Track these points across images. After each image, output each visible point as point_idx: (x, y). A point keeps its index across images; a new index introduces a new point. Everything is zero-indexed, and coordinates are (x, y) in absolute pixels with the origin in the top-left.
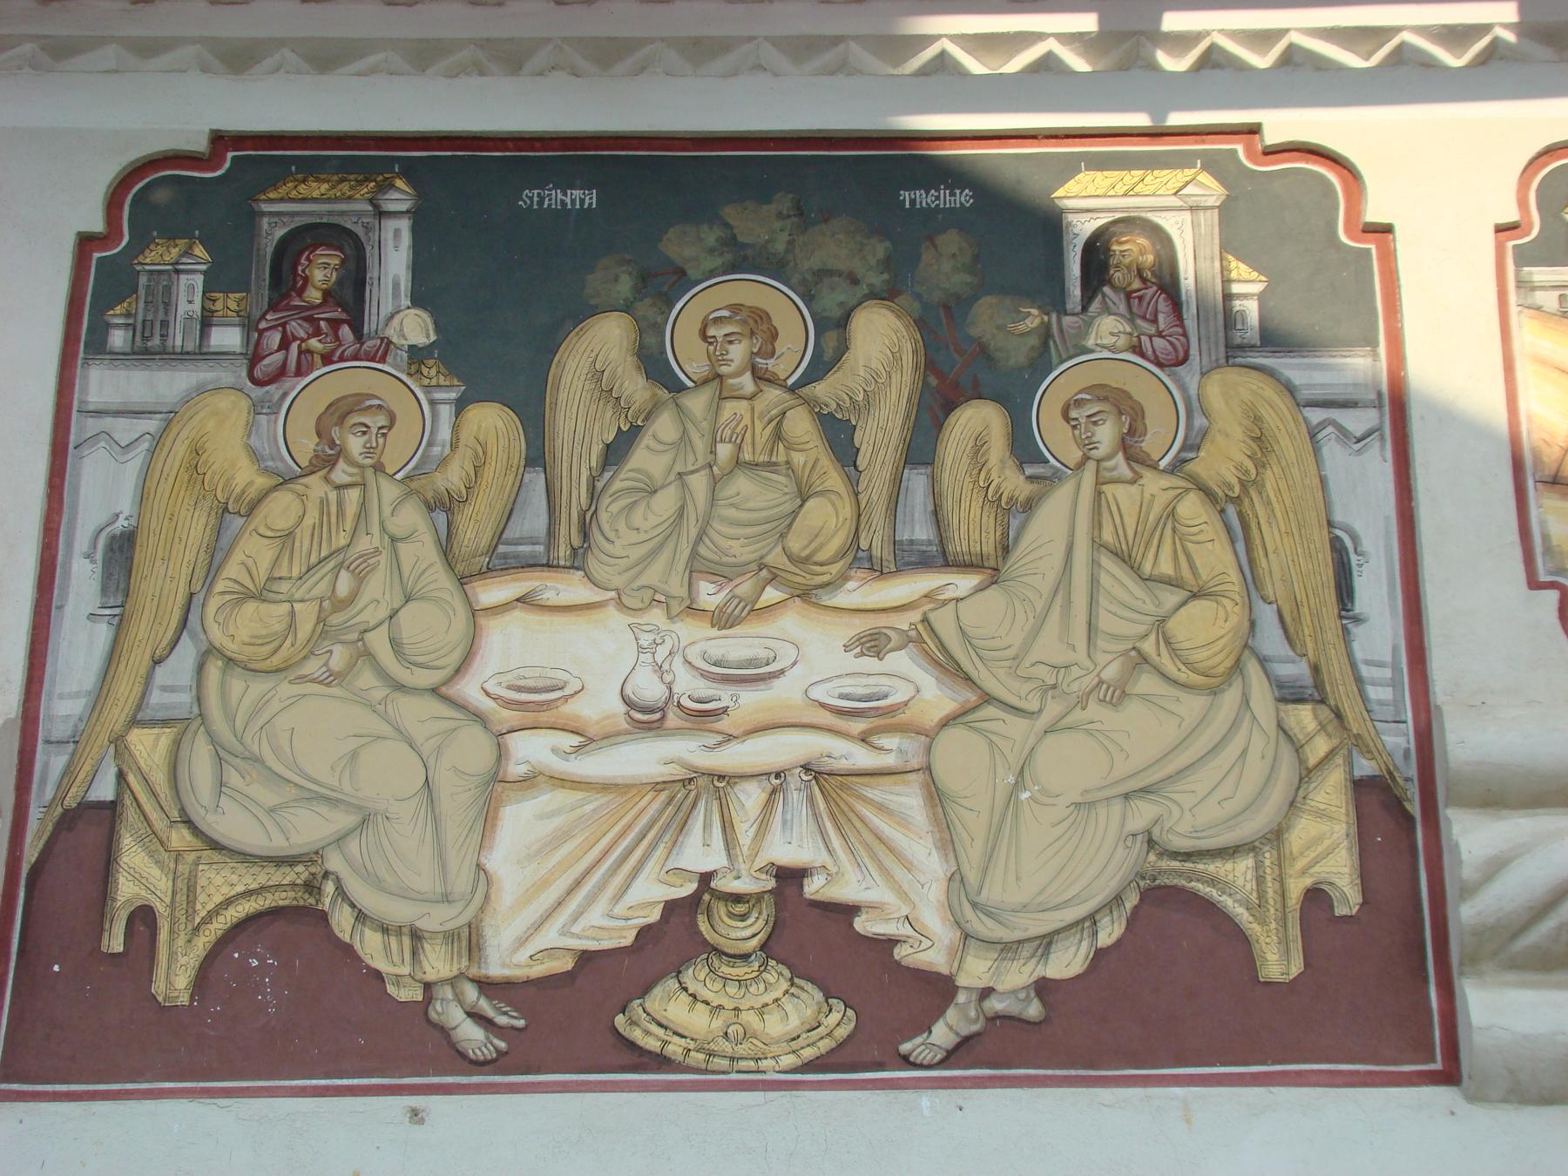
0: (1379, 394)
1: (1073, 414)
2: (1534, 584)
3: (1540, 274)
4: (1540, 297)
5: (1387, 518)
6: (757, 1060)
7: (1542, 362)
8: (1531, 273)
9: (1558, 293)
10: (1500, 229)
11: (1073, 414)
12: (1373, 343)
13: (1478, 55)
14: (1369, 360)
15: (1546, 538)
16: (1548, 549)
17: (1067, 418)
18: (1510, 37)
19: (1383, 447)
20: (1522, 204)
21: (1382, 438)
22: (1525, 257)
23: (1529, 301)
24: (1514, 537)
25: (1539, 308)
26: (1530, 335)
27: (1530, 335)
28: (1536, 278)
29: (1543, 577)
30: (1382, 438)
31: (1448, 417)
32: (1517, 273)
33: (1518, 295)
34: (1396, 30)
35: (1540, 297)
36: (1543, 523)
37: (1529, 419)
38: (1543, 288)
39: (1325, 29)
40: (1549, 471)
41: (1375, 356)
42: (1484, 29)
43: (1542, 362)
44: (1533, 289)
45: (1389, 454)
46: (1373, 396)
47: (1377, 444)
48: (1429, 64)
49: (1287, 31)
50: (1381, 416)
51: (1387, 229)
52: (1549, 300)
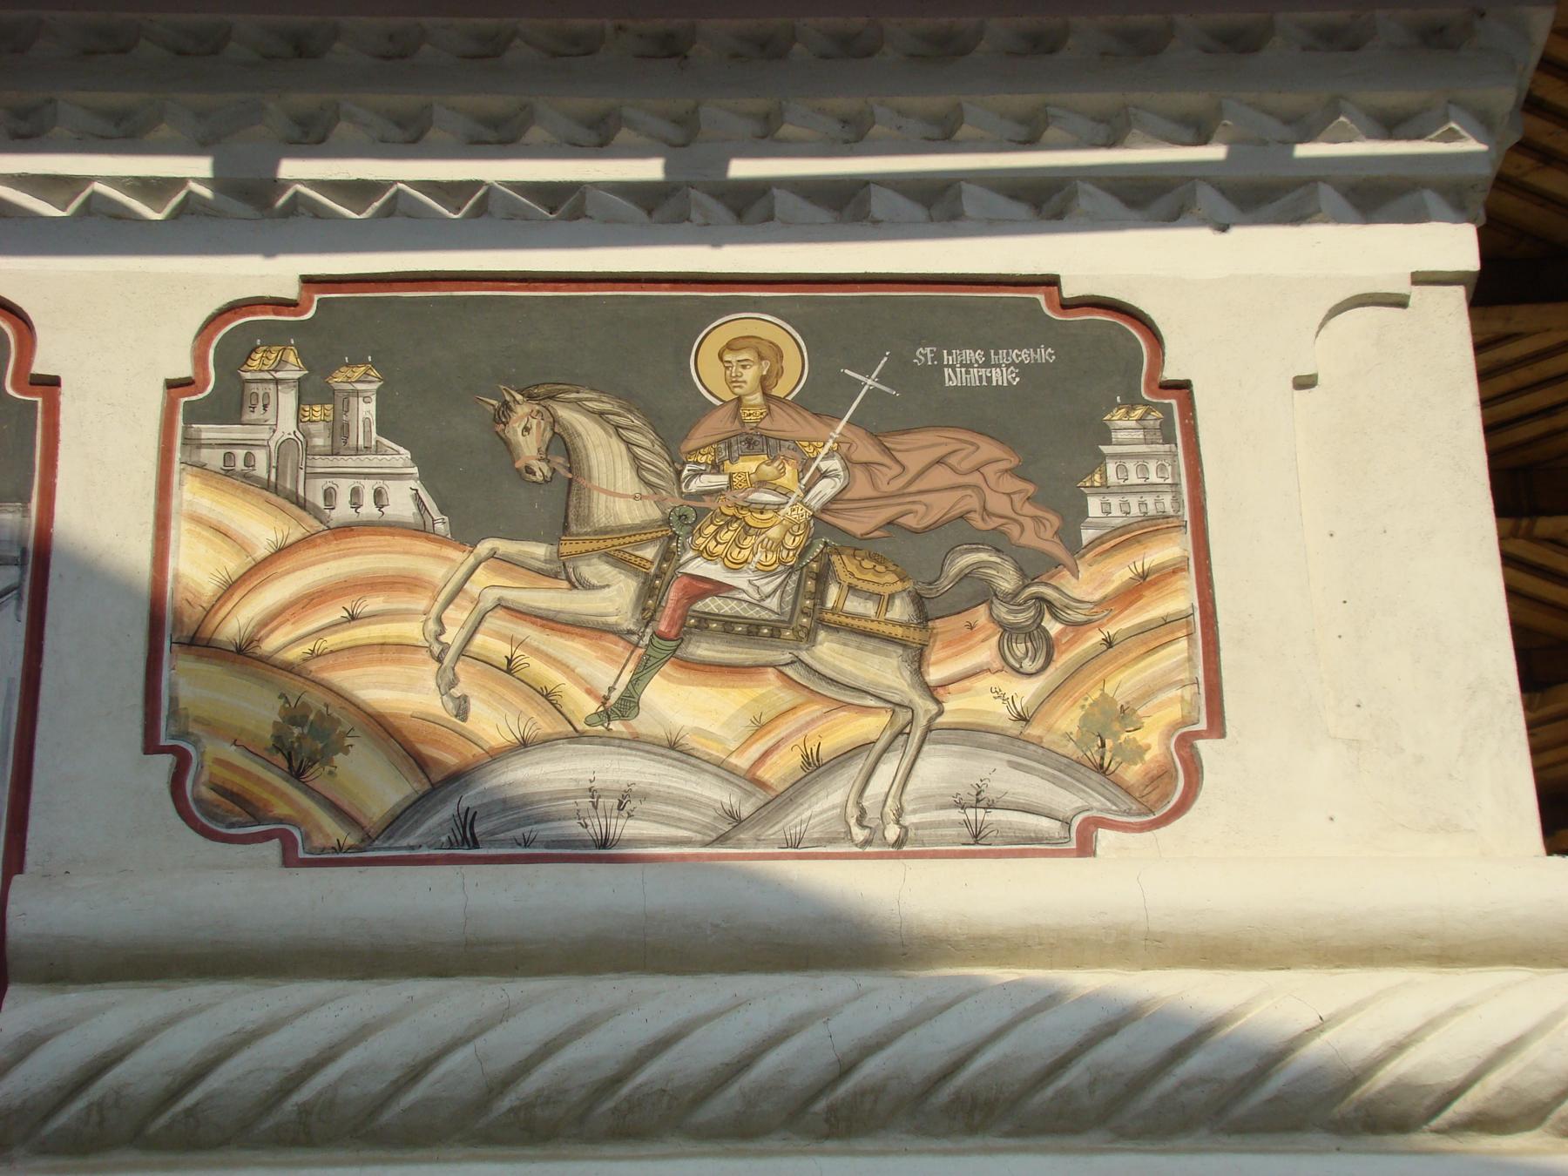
0: (24, 552)
1: (727, 357)
2: (151, 746)
3: (209, 432)
4: (205, 455)
5: (11, 681)
6: (510, 667)
7: (197, 520)
8: (200, 430)
9: (222, 452)
10: (172, 385)
11: (727, 357)
12: (26, 499)
13: (175, 209)
14: (18, 516)
15: (174, 700)
16: (174, 712)
17: (721, 358)
18: (206, 192)
19: (19, 607)
20: (199, 359)
21: (20, 598)
22: (196, 414)
23: (194, 459)
24: (137, 699)
25: (202, 467)
26: (190, 494)
27: (190, 494)
28: (204, 435)
29: (164, 741)
30: (20, 598)
31: (92, 573)
32: (185, 429)
33: (183, 453)
34: (89, 180)
35: (205, 455)
36: (173, 686)
37: (177, 577)
38: (210, 446)
39: (12, 176)
40: (187, 633)
41: (26, 511)
42: (180, 182)
43: (197, 520)
44: (200, 446)
45: (24, 614)
46: (16, 553)
47: (13, 603)
48: (121, 215)
49: (396, 182)
50: (23, 573)
51: (54, 382)
52: (214, 458)
